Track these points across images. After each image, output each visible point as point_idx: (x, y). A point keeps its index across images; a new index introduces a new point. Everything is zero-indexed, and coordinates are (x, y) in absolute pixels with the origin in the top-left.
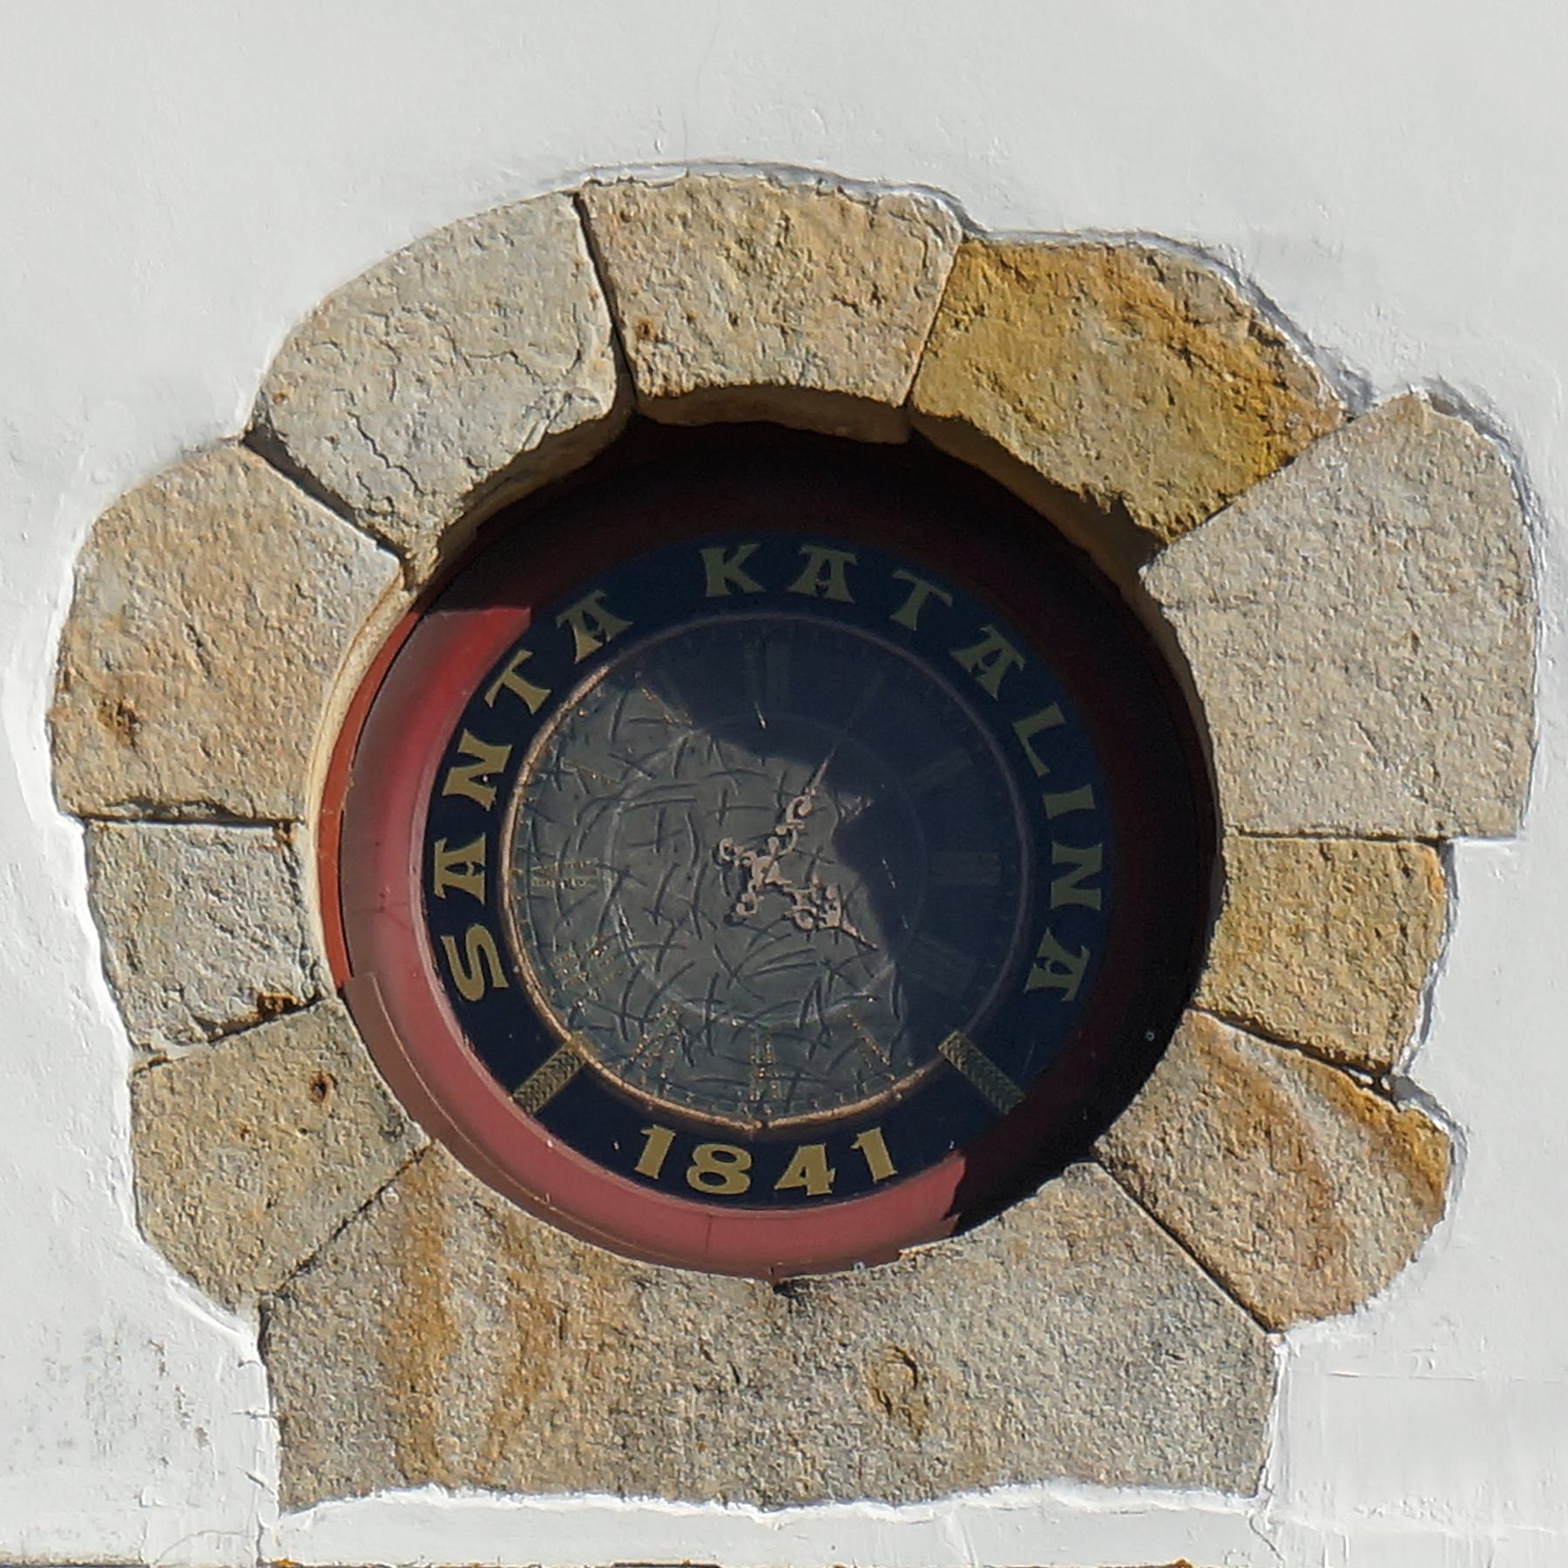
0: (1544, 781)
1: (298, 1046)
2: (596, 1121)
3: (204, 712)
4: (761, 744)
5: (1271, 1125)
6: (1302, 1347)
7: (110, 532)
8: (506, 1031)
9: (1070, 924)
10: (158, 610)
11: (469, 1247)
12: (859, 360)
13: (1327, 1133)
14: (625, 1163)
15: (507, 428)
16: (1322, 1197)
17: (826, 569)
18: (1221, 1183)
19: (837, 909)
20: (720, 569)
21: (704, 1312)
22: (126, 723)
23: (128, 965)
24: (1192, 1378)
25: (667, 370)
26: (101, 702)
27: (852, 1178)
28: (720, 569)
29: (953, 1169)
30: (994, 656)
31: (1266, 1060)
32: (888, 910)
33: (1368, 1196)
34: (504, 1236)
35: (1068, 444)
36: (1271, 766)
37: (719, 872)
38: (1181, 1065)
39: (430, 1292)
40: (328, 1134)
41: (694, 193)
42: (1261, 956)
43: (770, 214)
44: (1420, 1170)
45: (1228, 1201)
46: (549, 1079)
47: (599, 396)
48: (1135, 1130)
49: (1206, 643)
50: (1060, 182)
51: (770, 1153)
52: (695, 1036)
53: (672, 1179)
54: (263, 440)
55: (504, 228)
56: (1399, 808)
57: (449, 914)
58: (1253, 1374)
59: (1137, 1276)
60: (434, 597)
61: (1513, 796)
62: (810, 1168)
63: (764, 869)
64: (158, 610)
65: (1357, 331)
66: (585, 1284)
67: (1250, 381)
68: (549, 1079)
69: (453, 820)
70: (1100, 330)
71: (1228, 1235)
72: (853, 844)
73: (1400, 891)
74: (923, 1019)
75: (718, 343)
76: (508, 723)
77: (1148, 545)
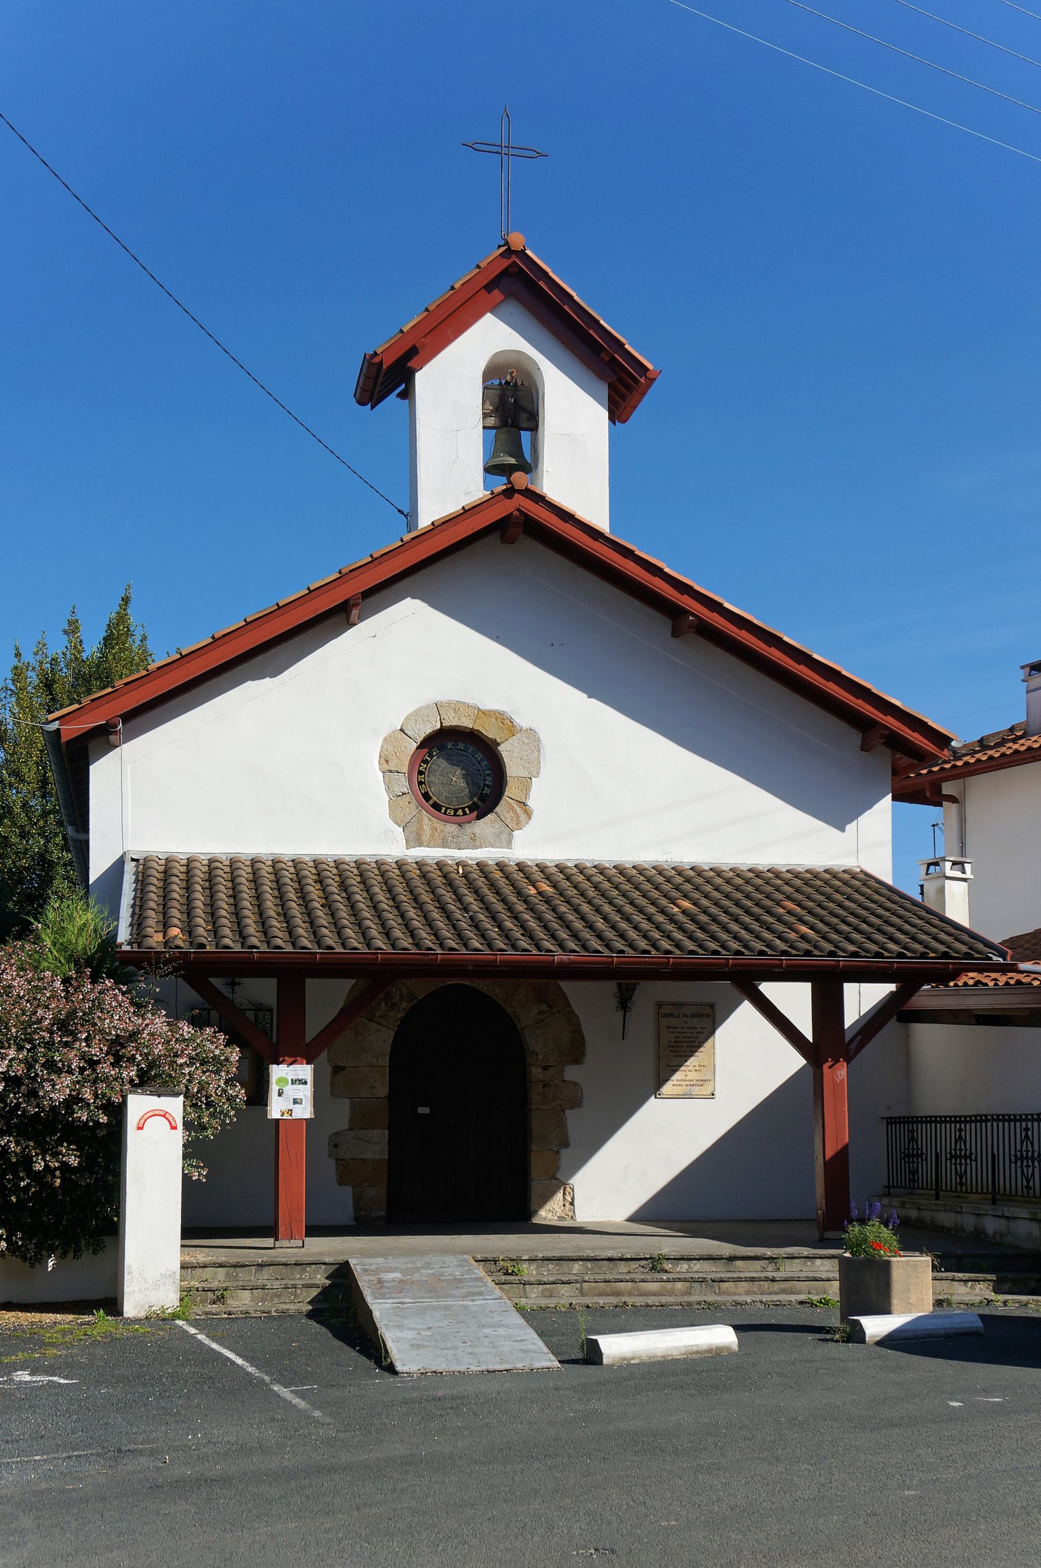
0: (803, 912)
1: (407, 798)
2: (437, 807)
3: (395, 760)
4: (454, 765)
5: (513, 809)
6: (516, 833)
7: (385, 740)
8: (427, 797)
9: (488, 786)
10: (391, 749)
11: (426, 821)
12: (467, 723)
13: (518, 810)
14: (440, 811)
15: (429, 730)
16: (518, 817)
17: (461, 746)
18: (507, 816)
19: (462, 784)
20: (449, 745)
21: (452, 828)
22: (387, 761)
23: (388, 788)
24: (504, 837)
25: (446, 724)
26: (384, 759)
27: (465, 814)
28: (449, 745)
29: (476, 813)
30: (479, 756)
31: (70, 970)
32: (468, 783)
33: (523, 817)
34: (430, 820)
35: (490, 732)
36: (512, 769)
37: (451, 778)
38: (502, 802)
39: (422, 826)
40: (410, 807)
41: (449, 703)
42: (511, 790)
43: (457, 706)
44: (529, 814)
45: (508, 817)
46: (431, 802)
47: (438, 726)
48: (498, 809)
49: (505, 755)
50: (489, 704)
51: (456, 810)
52: (447, 797)
53: (445, 813)
54: (402, 730)
55: (428, 707)
56: (526, 775)
57: (420, 783)
58: (511, 836)
59: (498, 825)
60: (418, 748)
61: (538, 773)
62: (460, 812)
63: (454, 779)
64: (391, 749)
65: (521, 721)
66: (438, 825)
67: (510, 727)
68: (431, 802)
69: (420, 773)
70: (493, 720)
71: (508, 821)
72: (464, 776)
73: (526, 783)
74: (472, 796)
75: (452, 720)
76: (426, 762)
77: (499, 744)
